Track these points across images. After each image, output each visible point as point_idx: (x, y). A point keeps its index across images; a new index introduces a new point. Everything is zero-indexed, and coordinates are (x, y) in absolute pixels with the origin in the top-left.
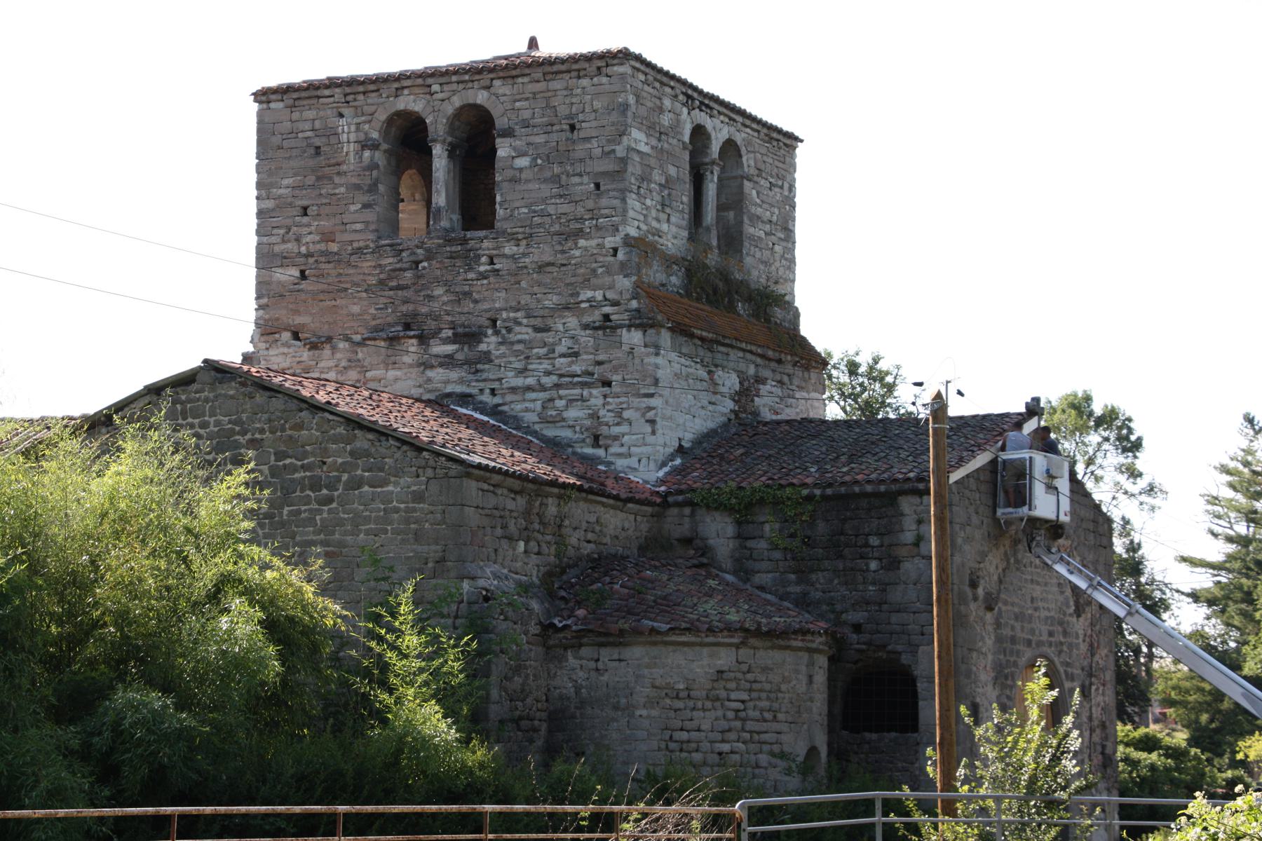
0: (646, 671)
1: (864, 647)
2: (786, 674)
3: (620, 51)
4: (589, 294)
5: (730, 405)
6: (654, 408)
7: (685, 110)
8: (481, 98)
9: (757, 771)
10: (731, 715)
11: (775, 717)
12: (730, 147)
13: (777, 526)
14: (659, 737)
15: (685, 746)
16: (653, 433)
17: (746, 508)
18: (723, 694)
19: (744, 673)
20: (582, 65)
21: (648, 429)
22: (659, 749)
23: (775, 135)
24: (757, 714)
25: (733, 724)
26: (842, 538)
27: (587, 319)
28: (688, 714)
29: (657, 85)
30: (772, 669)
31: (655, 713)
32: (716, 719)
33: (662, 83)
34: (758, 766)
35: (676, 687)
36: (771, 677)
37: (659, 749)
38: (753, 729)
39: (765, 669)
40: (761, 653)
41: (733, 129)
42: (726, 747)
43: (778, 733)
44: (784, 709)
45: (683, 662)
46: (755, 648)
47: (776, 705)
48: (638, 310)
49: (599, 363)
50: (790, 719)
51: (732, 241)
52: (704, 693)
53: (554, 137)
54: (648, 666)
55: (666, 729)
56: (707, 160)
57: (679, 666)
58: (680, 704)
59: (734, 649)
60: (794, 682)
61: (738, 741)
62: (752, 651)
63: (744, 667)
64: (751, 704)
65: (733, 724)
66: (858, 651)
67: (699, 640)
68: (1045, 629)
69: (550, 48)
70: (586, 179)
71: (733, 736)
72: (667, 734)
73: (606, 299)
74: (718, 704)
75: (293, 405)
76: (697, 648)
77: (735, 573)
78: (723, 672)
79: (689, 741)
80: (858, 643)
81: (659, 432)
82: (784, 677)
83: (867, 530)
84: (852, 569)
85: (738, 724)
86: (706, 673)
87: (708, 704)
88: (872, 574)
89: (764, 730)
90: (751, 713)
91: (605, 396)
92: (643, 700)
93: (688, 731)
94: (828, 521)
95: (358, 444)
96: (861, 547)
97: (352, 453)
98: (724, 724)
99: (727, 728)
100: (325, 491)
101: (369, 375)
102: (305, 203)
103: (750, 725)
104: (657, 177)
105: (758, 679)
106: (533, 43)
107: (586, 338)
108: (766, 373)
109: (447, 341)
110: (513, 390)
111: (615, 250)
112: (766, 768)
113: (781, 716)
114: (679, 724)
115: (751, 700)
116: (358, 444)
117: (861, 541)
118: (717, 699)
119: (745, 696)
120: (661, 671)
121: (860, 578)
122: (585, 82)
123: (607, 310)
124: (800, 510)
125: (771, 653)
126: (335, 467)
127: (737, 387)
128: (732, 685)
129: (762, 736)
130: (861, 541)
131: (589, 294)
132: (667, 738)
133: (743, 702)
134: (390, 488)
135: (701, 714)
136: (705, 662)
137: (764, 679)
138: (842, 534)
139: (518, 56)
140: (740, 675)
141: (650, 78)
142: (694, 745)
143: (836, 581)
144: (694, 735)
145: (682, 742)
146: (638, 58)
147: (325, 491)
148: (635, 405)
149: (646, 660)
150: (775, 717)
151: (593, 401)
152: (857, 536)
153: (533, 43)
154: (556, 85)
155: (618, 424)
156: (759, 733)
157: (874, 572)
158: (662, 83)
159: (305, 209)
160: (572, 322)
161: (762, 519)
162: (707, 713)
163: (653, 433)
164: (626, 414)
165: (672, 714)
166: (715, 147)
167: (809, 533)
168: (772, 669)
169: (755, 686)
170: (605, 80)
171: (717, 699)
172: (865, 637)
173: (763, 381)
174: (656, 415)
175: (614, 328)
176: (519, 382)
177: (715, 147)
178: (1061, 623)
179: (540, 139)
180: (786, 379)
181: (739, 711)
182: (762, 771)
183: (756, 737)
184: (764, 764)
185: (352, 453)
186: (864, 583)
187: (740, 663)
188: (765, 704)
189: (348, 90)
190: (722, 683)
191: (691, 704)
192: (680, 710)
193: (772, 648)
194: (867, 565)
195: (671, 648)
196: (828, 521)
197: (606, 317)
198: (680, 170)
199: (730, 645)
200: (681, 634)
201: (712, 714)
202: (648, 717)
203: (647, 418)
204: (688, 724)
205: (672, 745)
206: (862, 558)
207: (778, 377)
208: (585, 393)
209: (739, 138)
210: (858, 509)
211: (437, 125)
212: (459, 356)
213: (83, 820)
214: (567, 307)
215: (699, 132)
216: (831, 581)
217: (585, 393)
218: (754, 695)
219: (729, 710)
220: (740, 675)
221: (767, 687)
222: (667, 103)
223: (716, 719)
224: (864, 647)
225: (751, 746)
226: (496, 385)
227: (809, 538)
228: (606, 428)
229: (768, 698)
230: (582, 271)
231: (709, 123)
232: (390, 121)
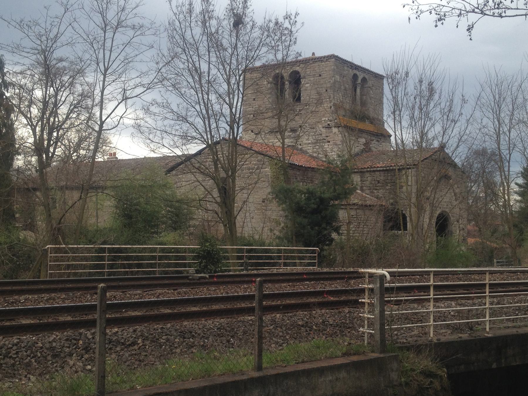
3: (332, 55)
4: (324, 119)
5: (363, 147)
7: (351, 70)
8: (297, 69)
12: (364, 80)
20: (322, 59)
23: (377, 76)
27: (324, 125)
29: (343, 63)
33: (344, 63)
41: (365, 75)
48: (337, 123)
49: (327, 137)
51: (363, 104)
53: (316, 78)
56: (358, 83)
68: (445, 204)
69: (318, 55)
70: (323, 89)
73: (328, 120)
75: (243, 148)
77: (360, 190)
91: (328, 145)
95: (259, 158)
97: (258, 161)
100: (251, 170)
101: (270, 141)
102: (254, 98)
104: (342, 87)
106: (313, 54)
107: (324, 130)
108: (374, 138)
109: (289, 132)
110: (306, 144)
111: (331, 107)
116: (259, 158)
122: (323, 63)
123: (329, 123)
126: (253, 164)
127: (365, 142)
131: (324, 119)
134: (267, 169)
139: (310, 57)
141: (341, 62)
146: (337, 57)
147: (251, 170)
153: (313, 54)
154: (316, 64)
158: (344, 63)
159: (254, 99)
160: (320, 126)
166: (359, 81)
170: (328, 62)
173: (373, 140)
175: (331, 127)
176: (307, 142)
177: (359, 81)
178: (451, 202)
179: (312, 79)
180: (379, 140)
185: (258, 161)
189: (264, 68)
197: (329, 125)
198: (349, 86)
207: (377, 139)
208: (323, 144)
209: (367, 77)
211: (286, 75)
212: (292, 136)
213: (447, 324)
214: (318, 122)
215: (355, 77)
217: (323, 144)
222: (346, 68)
226: (301, 143)
230: (322, 113)
231: (358, 73)
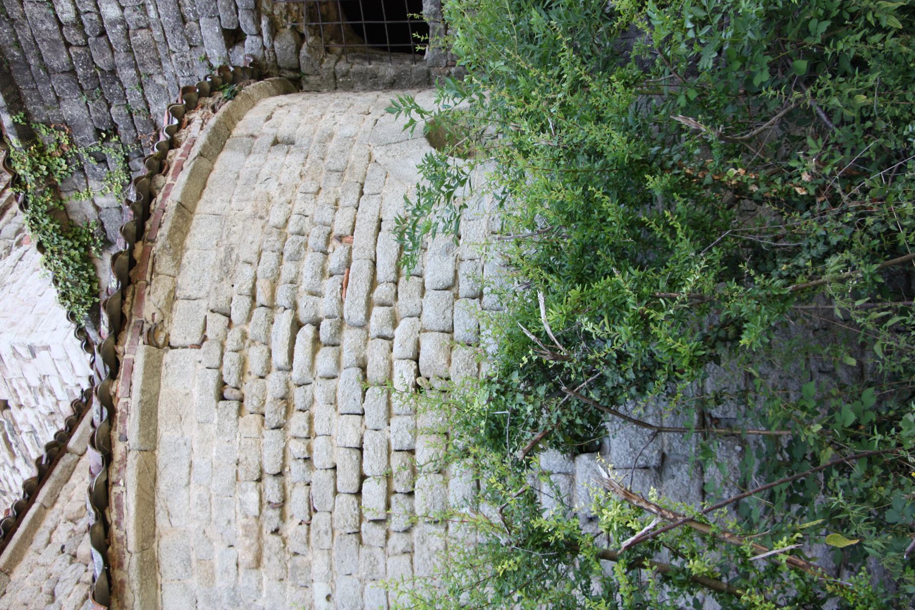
0: (222, 584)
1: (264, 22)
2: (249, 209)
6: (14, 348)
9: (465, 287)
10: (325, 361)
11: (340, 238)
13: (94, 184)
14: (378, 553)
15: (397, 486)
16: (47, 348)
17: (76, 237)
18: (274, 384)
19: (230, 325)
21: (42, 355)
22: (409, 552)
24: (330, 286)
25: (348, 357)
26: (80, 71)
28: (320, 477)
30: (230, 250)
31: (319, 565)
32: (334, 403)
34: (451, 286)
35: (254, 509)
36: (246, 252)
37: (409, 552)
38: (362, 301)
39: (226, 270)
40: (187, 283)
42: (404, 374)
43: (379, 229)
44: (327, 215)
45: (195, 492)
46: (172, 298)
47: (316, 238)
50: (352, 197)
52: (271, 436)
54: (210, 578)
55: (358, 533)
57: (206, 503)
58: (297, 506)
59: (168, 356)
60: (273, 188)
61: (390, 339)
62: (180, 305)
63: (217, 324)
64: (304, 302)
65: (348, 357)
66: (274, 30)
67: (133, 460)
71: (376, 355)
72: (371, 533)
74: (299, 397)
76: (161, 455)
78: (223, 384)
79: (388, 477)
80: (259, 34)
81: (46, 339)
82: (254, 215)
83: (50, 25)
84: (130, 51)
85: (350, 338)
86: (221, 431)
87: (297, 422)
88: (127, 12)
89: (366, 267)
90: (326, 306)
91: (20, 406)
92: (290, 591)
93: (363, 478)
94: (58, 99)
96: (86, 37)
98: (350, 376)
99: (356, 372)
103: (354, 311)
105: (246, 288)
112: (459, 260)
113: (341, 225)
114: (345, 503)
115: (295, 307)
117: (73, 36)
118: (286, 399)
119: (284, 320)
120: (219, 547)
121: (141, 36)
124: (52, 149)
125: (191, 255)
128: (255, 358)
129: (380, 276)
130: (73, 36)
132: (379, 531)
133: (297, 325)
135: (318, 444)
136: (193, 433)
137: (248, 271)
138: (73, 71)
140: (235, 335)
142: (397, 460)
143: (160, 80)
144: (373, 464)
145: (390, 492)
148: (18, 372)
149: (194, 582)
150: (340, 238)
151: (32, 421)
152: (68, 45)
155: (51, 392)
156: (373, 283)
157: (122, 8)
161: (91, 210)
162: (318, 427)
163: (47, 348)
164: (35, 383)
165: (320, 519)
167: (89, 132)
168: (230, 250)
169: (262, 297)
171: (286, 399)
172: (246, 23)
174: (22, 345)
181: (316, 340)
182: (465, 268)
183: (383, 291)
184: (449, 266)
186: (148, 27)
187: (205, 339)
188: (309, 263)
190: (251, 388)
191: (296, 470)
192: (309, 501)
193: (177, 249)
194: (113, 23)
195: (162, 522)
196: (58, 98)
199: (153, 371)
200: (119, 506)
201: (320, 410)
202: (330, 580)
203: (30, 356)
204: (347, 479)
205: (398, 522)
206: (103, 33)
210: (18, 43)
216: (160, 88)
218: (282, 299)
219: (312, 367)
220: (235, 335)
221: (269, 259)
223: (334, 403)
224: (264, 22)
225: (405, 304)
227: (98, 132)
228: (61, 404)
229: (296, 257)
232: (443, 150)
